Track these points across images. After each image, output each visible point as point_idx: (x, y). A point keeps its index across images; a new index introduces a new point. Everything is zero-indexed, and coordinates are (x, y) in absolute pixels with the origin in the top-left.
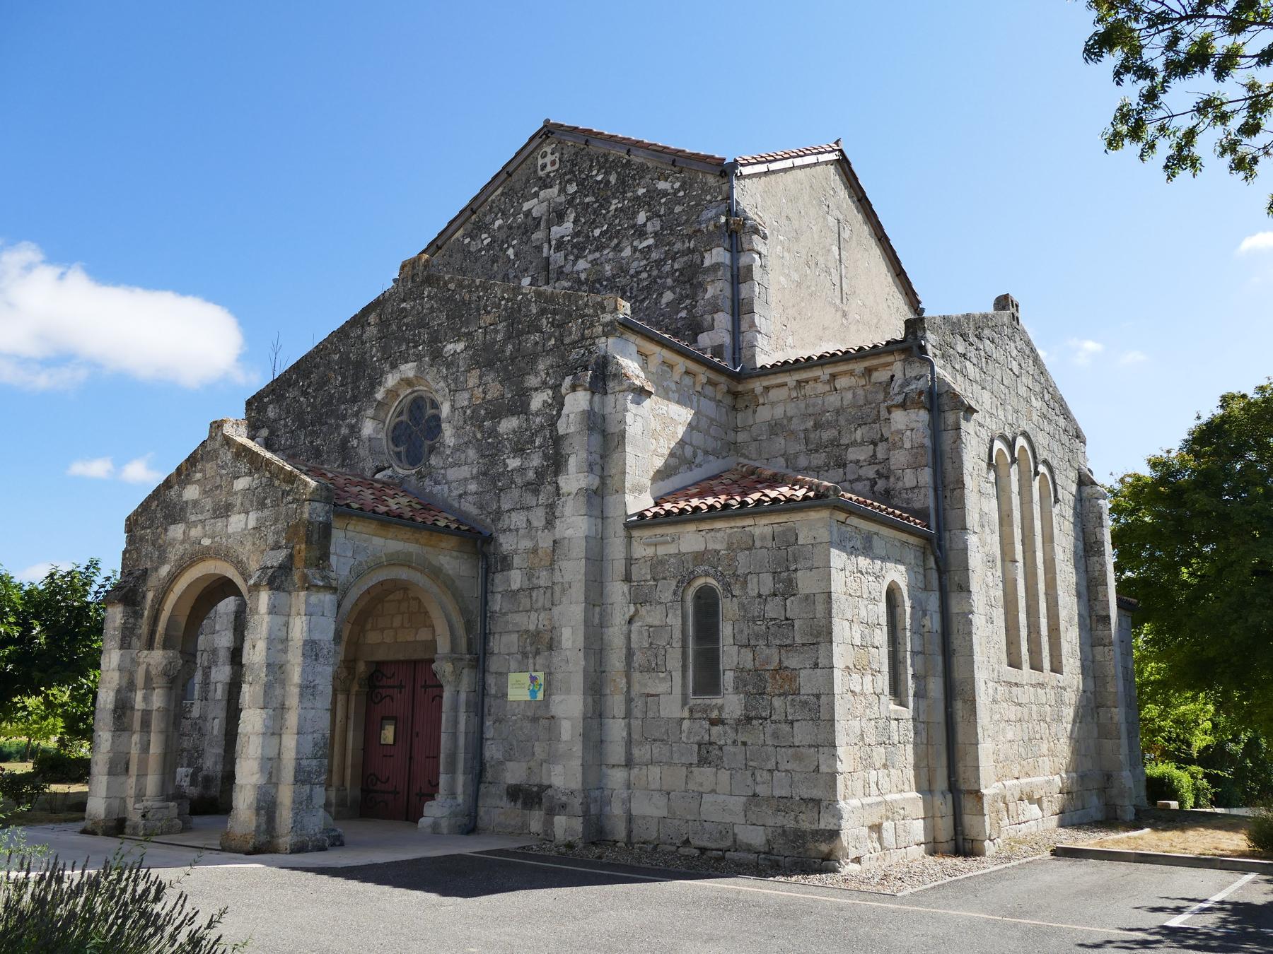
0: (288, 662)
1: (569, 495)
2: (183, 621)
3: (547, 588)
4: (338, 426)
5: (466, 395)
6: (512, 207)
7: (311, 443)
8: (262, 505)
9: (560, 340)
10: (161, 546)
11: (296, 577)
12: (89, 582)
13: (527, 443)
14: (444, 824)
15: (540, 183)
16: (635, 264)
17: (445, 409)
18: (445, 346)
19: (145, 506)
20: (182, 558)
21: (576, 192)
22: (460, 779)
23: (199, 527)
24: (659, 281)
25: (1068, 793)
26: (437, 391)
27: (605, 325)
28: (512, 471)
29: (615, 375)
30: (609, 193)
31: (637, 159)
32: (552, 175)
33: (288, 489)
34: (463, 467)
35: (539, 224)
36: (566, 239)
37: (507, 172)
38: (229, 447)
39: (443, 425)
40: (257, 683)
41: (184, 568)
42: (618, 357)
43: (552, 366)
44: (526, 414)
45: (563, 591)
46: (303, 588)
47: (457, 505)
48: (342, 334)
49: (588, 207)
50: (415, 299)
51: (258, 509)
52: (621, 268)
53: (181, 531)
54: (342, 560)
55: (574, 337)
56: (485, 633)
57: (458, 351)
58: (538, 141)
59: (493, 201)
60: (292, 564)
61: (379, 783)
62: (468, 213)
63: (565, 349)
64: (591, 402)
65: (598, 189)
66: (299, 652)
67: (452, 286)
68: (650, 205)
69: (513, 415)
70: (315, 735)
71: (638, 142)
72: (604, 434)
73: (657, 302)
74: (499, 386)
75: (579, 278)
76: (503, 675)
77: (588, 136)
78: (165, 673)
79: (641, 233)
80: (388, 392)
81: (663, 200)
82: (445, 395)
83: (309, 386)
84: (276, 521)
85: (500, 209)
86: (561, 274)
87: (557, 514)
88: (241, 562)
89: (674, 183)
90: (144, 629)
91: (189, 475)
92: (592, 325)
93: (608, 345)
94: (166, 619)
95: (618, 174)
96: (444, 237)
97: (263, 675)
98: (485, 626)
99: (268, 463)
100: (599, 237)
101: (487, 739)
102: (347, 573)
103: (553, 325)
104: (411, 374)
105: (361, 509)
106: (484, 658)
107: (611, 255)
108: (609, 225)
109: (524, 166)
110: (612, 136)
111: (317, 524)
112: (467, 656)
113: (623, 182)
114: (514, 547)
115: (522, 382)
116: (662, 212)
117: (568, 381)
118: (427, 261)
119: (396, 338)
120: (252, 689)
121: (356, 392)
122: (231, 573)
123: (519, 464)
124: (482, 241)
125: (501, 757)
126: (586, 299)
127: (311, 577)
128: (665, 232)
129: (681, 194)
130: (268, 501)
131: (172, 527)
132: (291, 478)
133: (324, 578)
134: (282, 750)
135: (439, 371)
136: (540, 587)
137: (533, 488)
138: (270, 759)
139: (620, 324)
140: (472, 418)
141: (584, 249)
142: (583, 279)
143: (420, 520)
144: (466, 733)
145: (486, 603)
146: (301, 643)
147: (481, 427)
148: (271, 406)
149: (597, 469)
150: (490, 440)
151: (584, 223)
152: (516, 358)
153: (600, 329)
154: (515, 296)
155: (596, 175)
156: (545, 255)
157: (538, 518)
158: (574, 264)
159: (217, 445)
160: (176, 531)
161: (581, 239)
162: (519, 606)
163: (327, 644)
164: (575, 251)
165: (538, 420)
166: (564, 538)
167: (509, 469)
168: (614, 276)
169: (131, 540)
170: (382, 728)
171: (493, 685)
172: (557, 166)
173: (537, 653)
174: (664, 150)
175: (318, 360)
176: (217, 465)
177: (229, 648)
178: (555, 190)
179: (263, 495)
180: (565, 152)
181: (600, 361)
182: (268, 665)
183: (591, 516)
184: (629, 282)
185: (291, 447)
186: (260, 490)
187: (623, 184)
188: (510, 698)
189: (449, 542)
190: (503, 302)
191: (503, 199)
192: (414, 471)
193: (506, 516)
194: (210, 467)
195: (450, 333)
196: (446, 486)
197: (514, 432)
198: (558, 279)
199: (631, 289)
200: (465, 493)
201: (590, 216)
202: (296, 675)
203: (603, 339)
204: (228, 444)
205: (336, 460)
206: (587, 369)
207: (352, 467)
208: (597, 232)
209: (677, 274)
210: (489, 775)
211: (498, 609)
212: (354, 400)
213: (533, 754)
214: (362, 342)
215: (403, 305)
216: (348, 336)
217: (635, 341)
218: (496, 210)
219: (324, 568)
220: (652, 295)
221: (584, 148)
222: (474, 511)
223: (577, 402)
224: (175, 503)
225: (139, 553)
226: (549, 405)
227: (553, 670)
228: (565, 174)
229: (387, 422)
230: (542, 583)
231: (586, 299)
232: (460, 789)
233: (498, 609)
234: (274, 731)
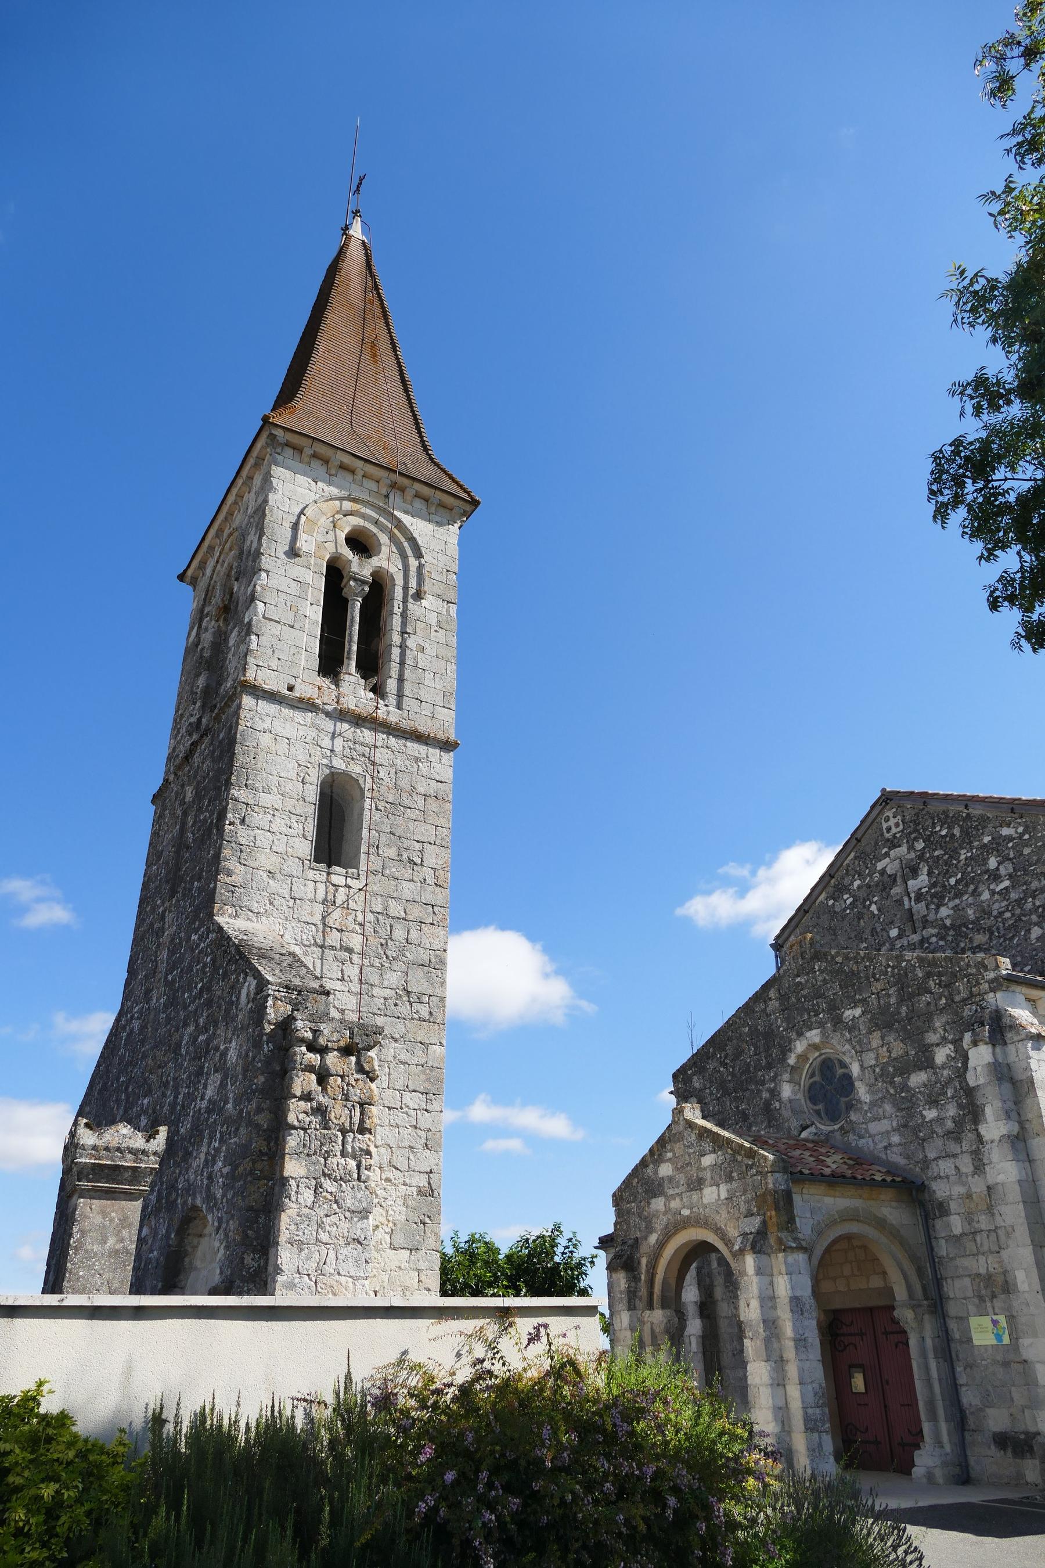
0: (779, 1317)
1: (992, 1142)
2: (673, 1282)
3: (989, 1231)
4: (759, 1091)
5: (872, 1055)
6: (867, 868)
7: (737, 1107)
8: (730, 1179)
9: (950, 998)
10: (646, 1218)
11: (772, 1241)
12: (554, 1245)
13: (940, 1094)
14: (938, 1474)
15: (889, 844)
16: (996, 906)
17: (855, 1069)
18: (843, 1012)
19: (627, 1183)
20: (666, 1227)
22: (944, 1427)
23: (678, 1200)
24: (1023, 918)
25: (580, 1265)
26: (844, 1053)
27: (991, 982)
28: (931, 1121)
29: (1011, 1027)
30: (956, 845)
31: (976, 811)
32: (898, 835)
34: (883, 1121)
35: (895, 880)
36: (924, 890)
37: (856, 839)
38: (692, 1130)
39: (856, 1084)
40: (757, 1338)
41: (670, 1236)
42: (1009, 1009)
43: (948, 1023)
44: (932, 1068)
45: (1008, 1235)
46: (780, 1251)
47: (884, 1157)
48: (747, 1009)
49: (938, 860)
50: (808, 974)
51: (727, 1182)
52: (984, 911)
53: (662, 1204)
54: (804, 1220)
55: (964, 994)
56: (937, 1279)
57: (857, 1016)
58: (878, 808)
59: (848, 865)
60: (766, 1229)
62: (827, 878)
63: (957, 1007)
64: (994, 1054)
65: (945, 843)
66: (788, 1308)
67: (839, 959)
68: (998, 851)
69: (920, 1070)
70: (814, 1385)
71: (973, 797)
72: (1013, 1082)
73: (1026, 938)
74: (901, 1045)
75: (945, 925)
76: (963, 1320)
77: (925, 798)
78: (667, 1331)
79: (995, 876)
81: (1010, 845)
82: (852, 1057)
83: (726, 1058)
84: (745, 1192)
85: (856, 871)
86: (925, 923)
87: (985, 1161)
88: (720, 1228)
89: (1017, 828)
90: (643, 1292)
91: (660, 1155)
92: (978, 983)
93: (997, 999)
94: (661, 1281)
95: (961, 827)
96: (810, 901)
97: (761, 1330)
99: (729, 1141)
100: (955, 885)
101: (961, 1385)
102: (809, 1232)
103: (940, 986)
104: (817, 1040)
105: (812, 1174)
106: (941, 1304)
107: (971, 900)
109: (870, 831)
110: (947, 795)
111: (780, 1192)
112: (925, 1302)
113: (968, 834)
114: (948, 1193)
115: (923, 1039)
116: (1012, 855)
117: (968, 1037)
118: (811, 939)
119: (797, 1009)
120: (753, 1344)
121: (770, 1059)
122: (711, 1238)
123: (936, 1114)
124: (845, 901)
125: (979, 1403)
126: (966, 960)
127: (785, 1240)
128: (1019, 873)
129: (1027, 837)
130: (735, 1174)
131: (654, 1201)
132: (751, 1154)
133: (795, 1239)
134: (789, 1400)
135: (843, 1036)
136: (982, 1231)
137: (955, 1135)
138: (780, 1408)
139: (1004, 979)
140: (882, 1075)
141: (943, 897)
142: (948, 925)
143: (860, 1177)
144: (940, 1380)
145: (932, 1249)
146: (787, 1300)
147: (892, 1083)
148: (695, 1077)
149: (1014, 1115)
150: (903, 1094)
151: (938, 874)
152: (912, 1018)
153: (986, 986)
154: (900, 963)
155: (940, 830)
156: (907, 907)
157: (966, 1164)
158: (937, 912)
159: (681, 1128)
160: (658, 1204)
161: (938, 889)
162: (965, 1252)
163: (808, 1299)
164: (935, 900)
165: (945, 1073)
166: (997, 1184)
167: (927, 1120)
168: (977, 919)
169: (619, 1213)
170: (851, 1377)
171: (955, 1330)
172: (901, 827)
173: (994, 1296)
174: (1000, 801)
175: (730, 1033)
176: (685, 1146)
177: (696, 1302)
178: (904, 849)
179: (729, 1169)
180: (905, 814)
181: (993, 1015)
182: (764, 1321)
183: (1018, 1161)
184: (994, 922)
185: (719, 1112)
186: (726, 1165)
187: (968, 837)
188: (976, 1342)
189: (887, 1195)
190: (889, 970)
191: (857, 862)
192: (836, 1127)
193: (934, 1164)
194: (678, 1147)
195: (845, 1001)
196: (870, 1139)
197: (925, 1085)
198: (924, 928)
199: (998, 929)
200: (890, 1145)
201: (941, 868)
202: (788, 1329)
203: (991, 995)
204: (690, 1127)
205: (762, 1122)
206: (983, 1025)
207: (779, 1128)
208: (952, 881)
209: (1040, 910)
210: (971, 1422)
211: (945, 1254)
212: (769, 1066)
213: (1012, 1400)
214: (767, 1015)
215: (798, 979)
216: (753, 1011)
217: (1021, 992)
218: (852, 872)
219: (793, 1231)
220: (1019, 933)
221: (923, 809)
222: (902, 1161)
223: (981, 1056)
224: (653, 1180)
225: (628, 1224)
226: (953, 1058)
227: (1015, 1314)
228: (910, 833)
229: (802, 1083)
230: (983, 1227)
231: (966, 960)
232: (945, 1438)
233: (945, 1254)
234: (779, 1382)
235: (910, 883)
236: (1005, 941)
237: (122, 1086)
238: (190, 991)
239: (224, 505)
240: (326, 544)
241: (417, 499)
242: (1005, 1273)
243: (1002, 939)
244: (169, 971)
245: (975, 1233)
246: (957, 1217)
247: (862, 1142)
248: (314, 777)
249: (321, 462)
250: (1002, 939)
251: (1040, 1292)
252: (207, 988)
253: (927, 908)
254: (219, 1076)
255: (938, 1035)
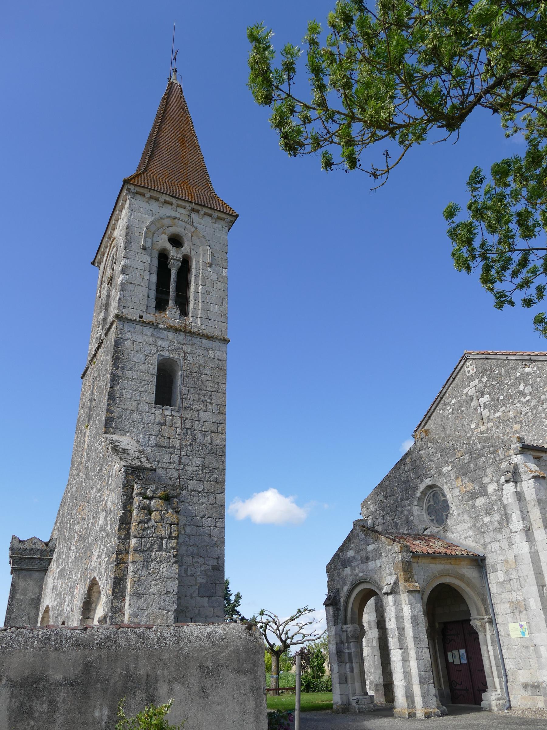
2: (357, 611)
4: (403, 511)
13: (491, 509)
20: (352, 582)
21: (487, 381)
24: (538, 415)
32: (473, 375)
33: (390, 548)
35: (473, 398)
54: (419, 577)
61: (458, 685)
74: (471, 484)
80: (422, 493)
84: (389, 562)
86: (489, 419)
90: (341, 616)
97: (397, 633)
98: (491, 600)
108: (507, 393)
123: (489, 520)
124: (448, 411)
137: (499, 530)
148: (372, 505)
152: (476, 470)
156: (479, 412)
157: (504, 544)
160: (348, 571)
164: (493, 408)
165: (493, 498)
188: (512, 636)
190: (464, 445)
193: (489, 546)
197: (483, 505)
198: (488, 422)
199: (525, 421)
223: (510, 488)
234: (405, 660)
235: (481, 399)
236: (528, 428)
237: (68, 520)
238: (94, 472)
239: (109, 226)
240: (158, 243)
241: (206, 217)
242: (524, 600)
243: (527, 427)
244: (86, 462)
245: (510, 580)
246: (501, 572)
247: (454, 536)
248: (155, 360)
249: (155, 201)
250: (527, 427)
251: (542, 609)
252: (101, 470)
253: (489, 412)
254: (104, 513)
255: (489, 478)
